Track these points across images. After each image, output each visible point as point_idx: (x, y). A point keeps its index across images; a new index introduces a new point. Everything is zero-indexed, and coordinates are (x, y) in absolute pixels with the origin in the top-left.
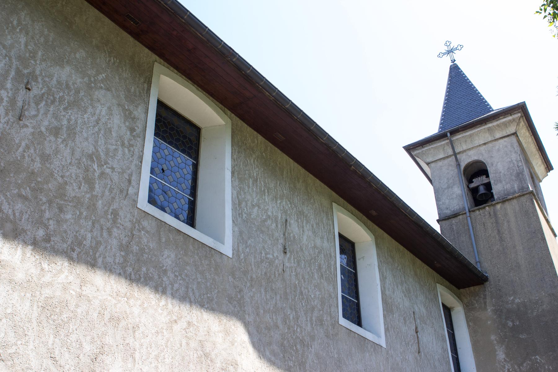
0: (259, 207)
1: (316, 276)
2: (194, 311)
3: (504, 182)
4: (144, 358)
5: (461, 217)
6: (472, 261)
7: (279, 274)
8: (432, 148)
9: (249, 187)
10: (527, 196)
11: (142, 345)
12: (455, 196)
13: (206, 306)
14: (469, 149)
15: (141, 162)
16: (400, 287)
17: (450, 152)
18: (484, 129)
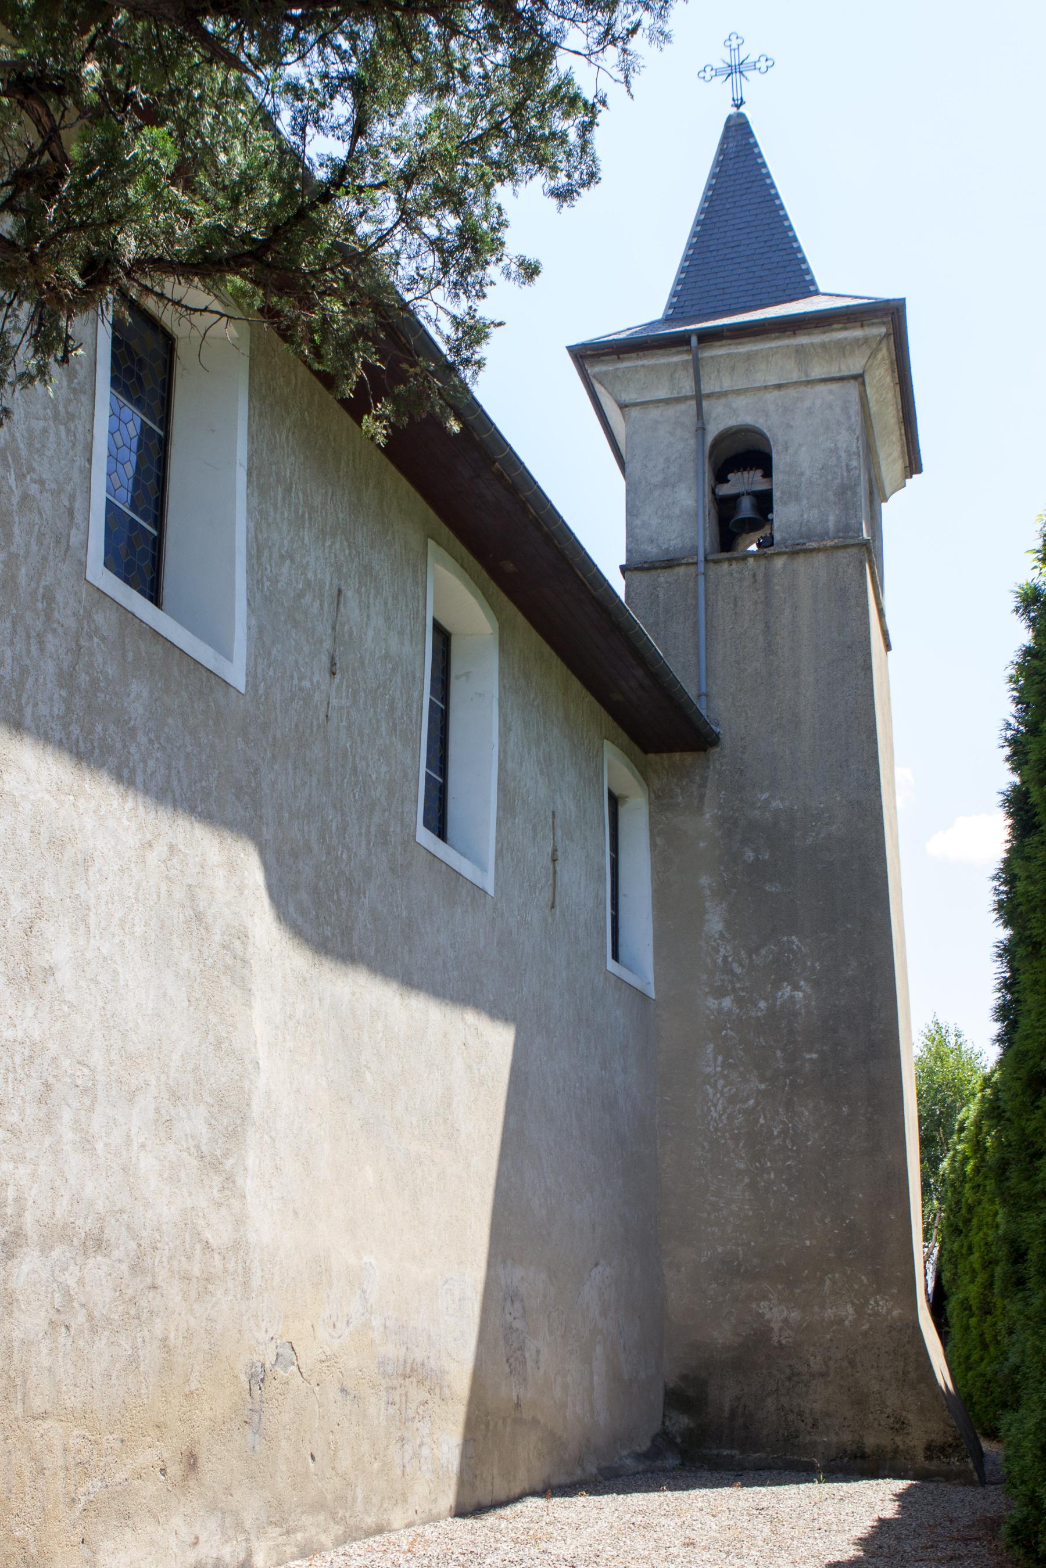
0: (293, 561)
1: (383, 729)
2: (180, 822)
3: (805, 502)
4: (103, 924)
5: (681, 570)
6: (692, 692)
7: (319, 726)
8: (643, 366)
9: (276, 508)
10: (853, 551)
11: (98, 898)
12: (677, 511)
13: (199, 809)
14: (737, 392)
15: (90, 461)
16: (534, 751)
17: (687, 387)
18: (788, 346)
